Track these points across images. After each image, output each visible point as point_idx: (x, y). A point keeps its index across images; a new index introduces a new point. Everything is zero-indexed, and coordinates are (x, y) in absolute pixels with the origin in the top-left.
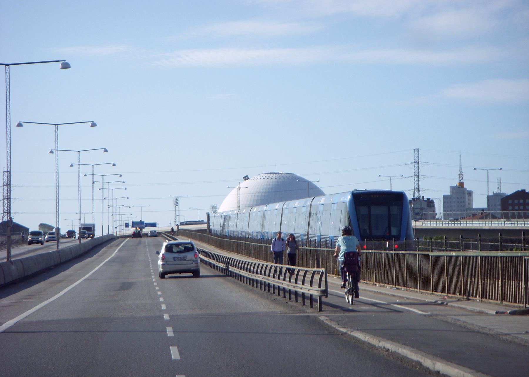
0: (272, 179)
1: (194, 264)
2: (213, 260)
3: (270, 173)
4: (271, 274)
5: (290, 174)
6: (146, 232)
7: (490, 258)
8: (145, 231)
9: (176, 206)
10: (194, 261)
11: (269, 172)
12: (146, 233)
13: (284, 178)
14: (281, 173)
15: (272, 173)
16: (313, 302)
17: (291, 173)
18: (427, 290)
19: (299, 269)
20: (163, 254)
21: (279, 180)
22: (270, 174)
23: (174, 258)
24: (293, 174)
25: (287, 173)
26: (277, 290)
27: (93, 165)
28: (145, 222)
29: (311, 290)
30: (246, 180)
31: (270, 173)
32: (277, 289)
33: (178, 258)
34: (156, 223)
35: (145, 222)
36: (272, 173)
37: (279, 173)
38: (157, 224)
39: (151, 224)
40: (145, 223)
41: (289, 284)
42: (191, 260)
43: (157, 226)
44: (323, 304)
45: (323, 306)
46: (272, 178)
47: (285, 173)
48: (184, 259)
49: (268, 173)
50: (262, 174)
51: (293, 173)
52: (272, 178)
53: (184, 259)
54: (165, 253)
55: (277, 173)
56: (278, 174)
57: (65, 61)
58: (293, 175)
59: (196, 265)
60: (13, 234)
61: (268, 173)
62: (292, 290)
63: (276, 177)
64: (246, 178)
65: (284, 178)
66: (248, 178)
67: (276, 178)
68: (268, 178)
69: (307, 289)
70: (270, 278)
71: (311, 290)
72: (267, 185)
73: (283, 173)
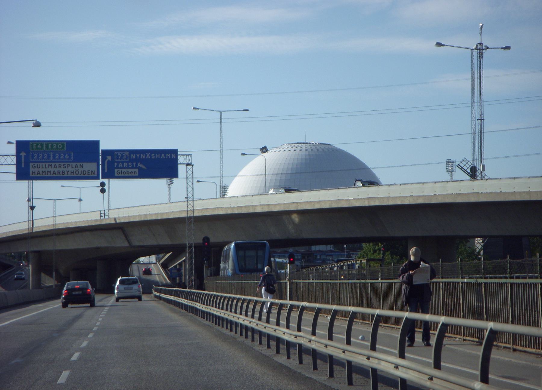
0: (295, 151)
1: (137, 292)
2: (204, 304)
3: (298, 143)
4: (262, 317)
5: (326, 144)
6: (119, 218)
7: (456, 284)
8: (116, 216)
9: (169, 184)
10: (138, 290)
11: (296, 142)
12: (118, 221)
13: (318, 150)
14: (313, 143)
15: (300, 143)
16: (271, 341)
17: (327, 143)
18: (392, 324)
19: (206, 293)
20: (118, 286)
21: (311, 153)
22: (297, 145)
23: (125, 288)
24: (329, 145)
25: (321, 144)
26: (265, 338)
27: (55, 200)
28: (103, 147)
29: (330, 346)
30: (264, 152)
31: (298, 143)
32: (266, 337)
33: (127, 288)
34: (175, 152)
35: (103, 147)
36: (300, 143)
37: (310, 143)
38: (181, 159)
39: (143, 161)
40: (106, 153)
41: (259, 322)
42: (136, 290)
43: (182, 169)
44: (272, 340)
45: (354, 376)
46: (301, 150)
47: (318, 144)
48: (132, 289)
49: (295, 144)
50: (287, 144)
51: (329, 143)
52: (301, 150)
53: (132, 289)
54: (119, 285)
55: (307, 143)
56: (309, 145)
57: (36, 120)
58: (330, 146)
59: (139, 292)
60: (353, 270)
61: (295, 144)
62: (353, 364)
63: (307, 149)
64: (264, 150)
65: (318, 150)
66: (267, 151)
67: (306, 150)
68: (295, 150)
69: (282, 331)
70: (254, 320)
71: (330, 346)
72: (302, 159)
73: (316, 143)
